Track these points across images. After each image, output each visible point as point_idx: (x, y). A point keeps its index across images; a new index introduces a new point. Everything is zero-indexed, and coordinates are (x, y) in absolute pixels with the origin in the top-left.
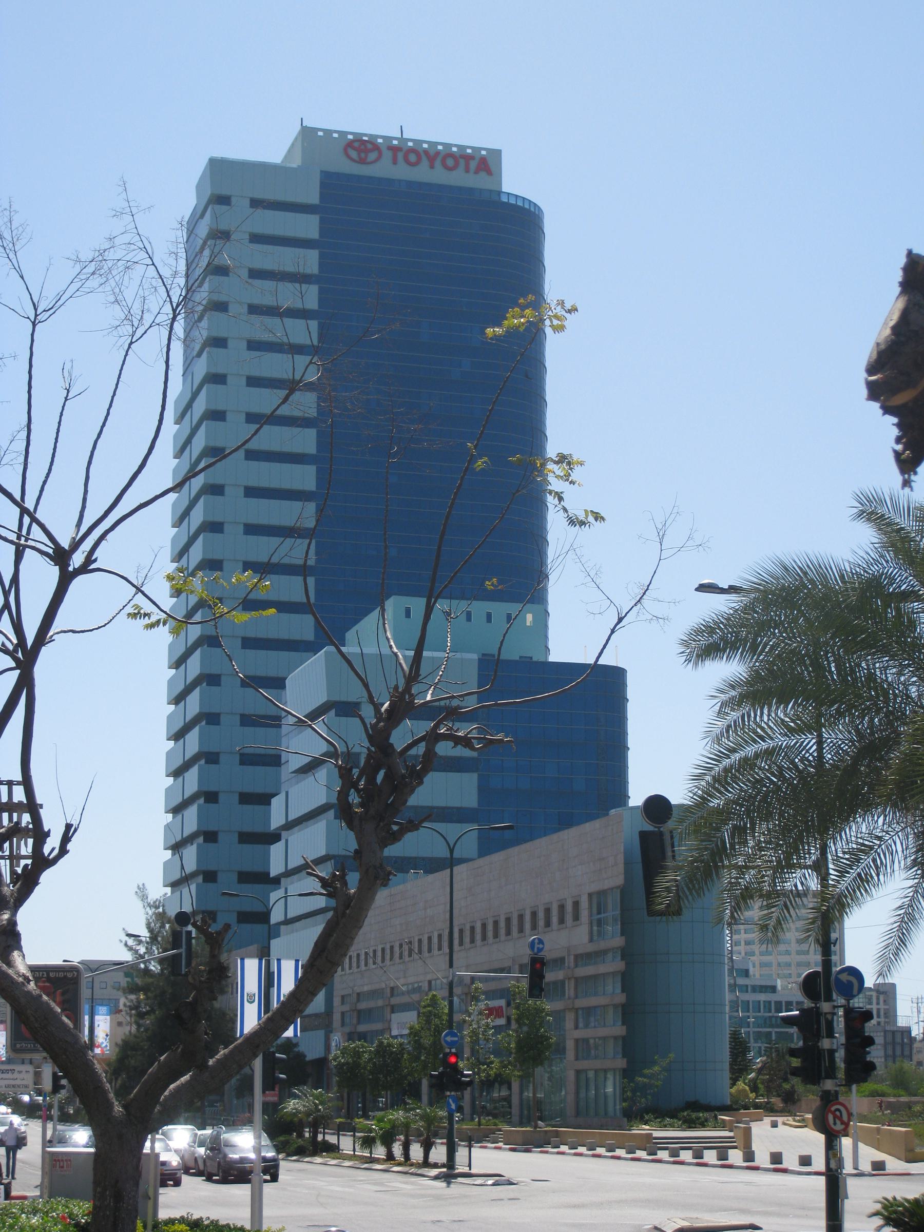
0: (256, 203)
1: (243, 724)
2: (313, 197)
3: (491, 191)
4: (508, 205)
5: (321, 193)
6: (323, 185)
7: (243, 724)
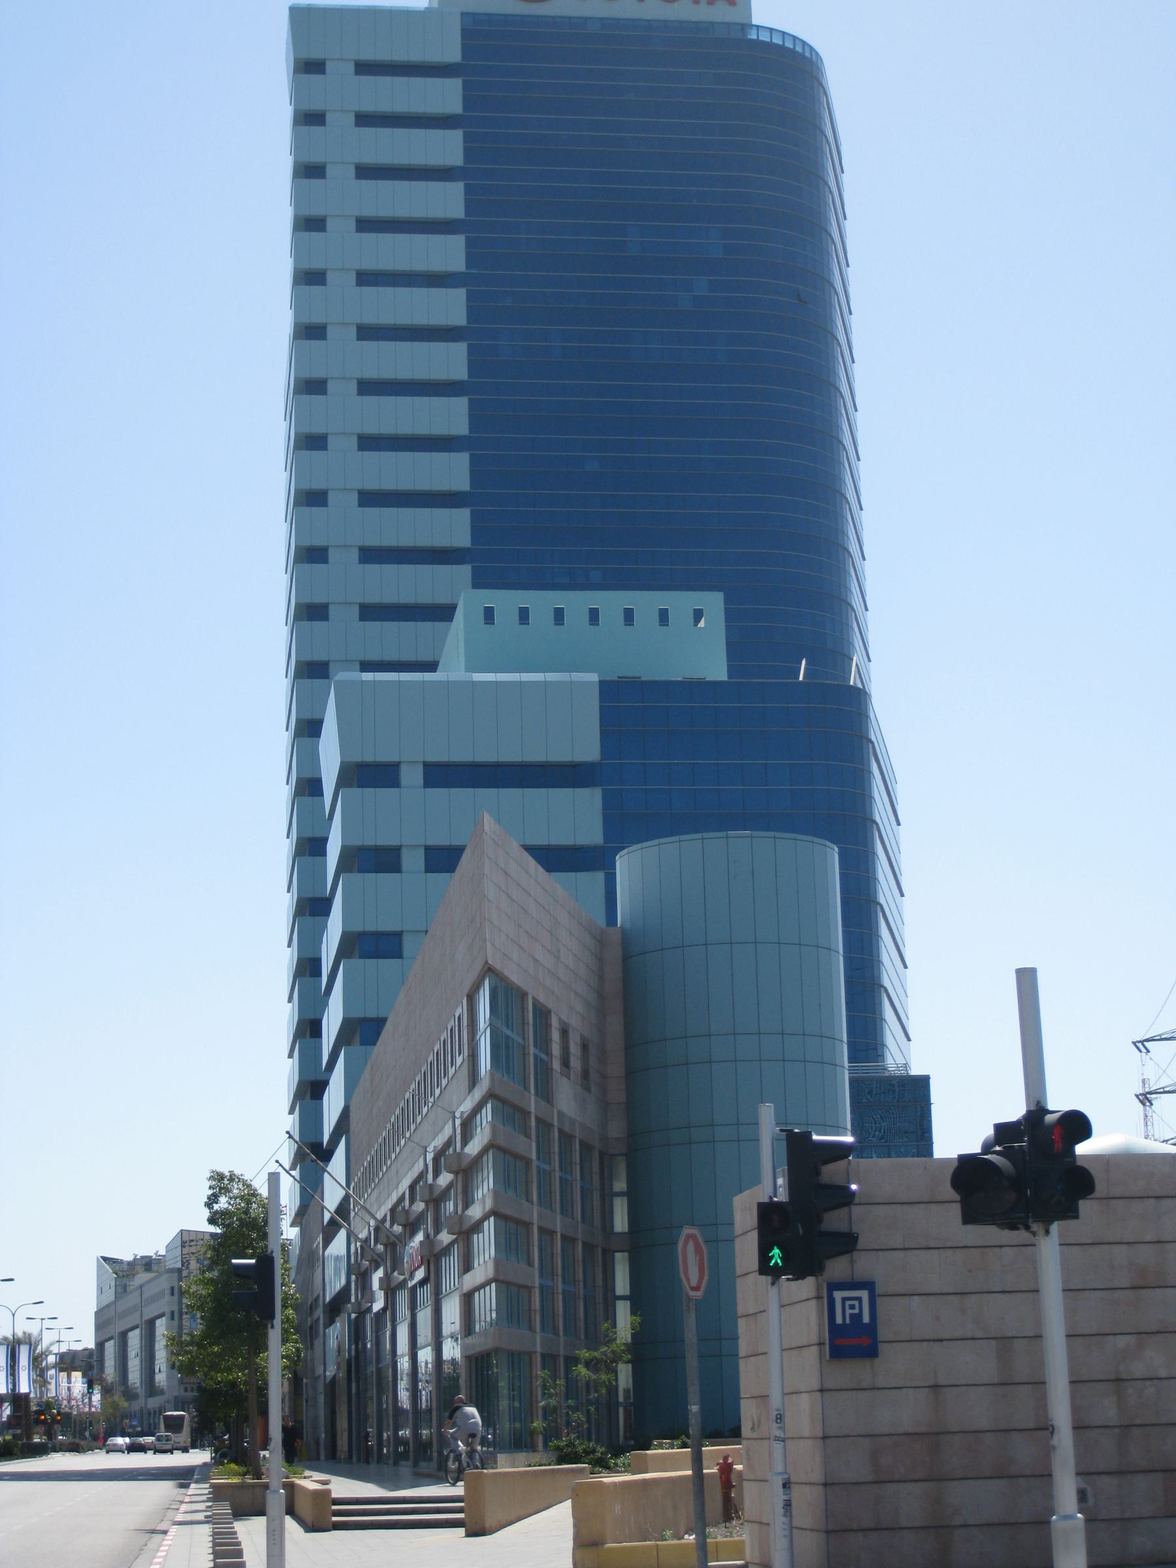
0: (364, 68)
1: (360, 337)
2: (452, 53)
3: (729, 24)
4: (758, 43)
5: (466, 149)
6: (466, 34)
7: (360, 337)
